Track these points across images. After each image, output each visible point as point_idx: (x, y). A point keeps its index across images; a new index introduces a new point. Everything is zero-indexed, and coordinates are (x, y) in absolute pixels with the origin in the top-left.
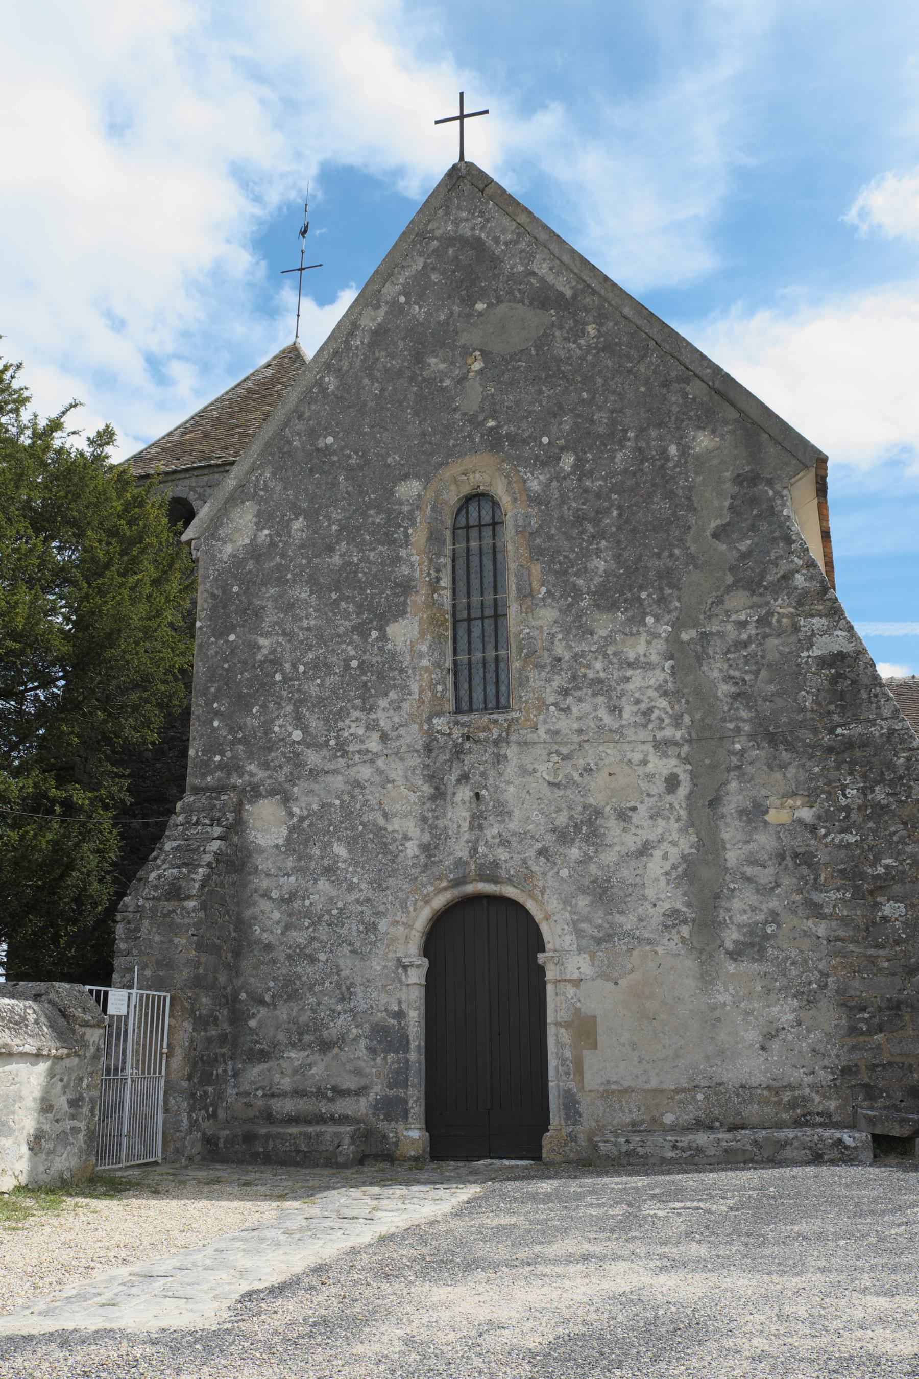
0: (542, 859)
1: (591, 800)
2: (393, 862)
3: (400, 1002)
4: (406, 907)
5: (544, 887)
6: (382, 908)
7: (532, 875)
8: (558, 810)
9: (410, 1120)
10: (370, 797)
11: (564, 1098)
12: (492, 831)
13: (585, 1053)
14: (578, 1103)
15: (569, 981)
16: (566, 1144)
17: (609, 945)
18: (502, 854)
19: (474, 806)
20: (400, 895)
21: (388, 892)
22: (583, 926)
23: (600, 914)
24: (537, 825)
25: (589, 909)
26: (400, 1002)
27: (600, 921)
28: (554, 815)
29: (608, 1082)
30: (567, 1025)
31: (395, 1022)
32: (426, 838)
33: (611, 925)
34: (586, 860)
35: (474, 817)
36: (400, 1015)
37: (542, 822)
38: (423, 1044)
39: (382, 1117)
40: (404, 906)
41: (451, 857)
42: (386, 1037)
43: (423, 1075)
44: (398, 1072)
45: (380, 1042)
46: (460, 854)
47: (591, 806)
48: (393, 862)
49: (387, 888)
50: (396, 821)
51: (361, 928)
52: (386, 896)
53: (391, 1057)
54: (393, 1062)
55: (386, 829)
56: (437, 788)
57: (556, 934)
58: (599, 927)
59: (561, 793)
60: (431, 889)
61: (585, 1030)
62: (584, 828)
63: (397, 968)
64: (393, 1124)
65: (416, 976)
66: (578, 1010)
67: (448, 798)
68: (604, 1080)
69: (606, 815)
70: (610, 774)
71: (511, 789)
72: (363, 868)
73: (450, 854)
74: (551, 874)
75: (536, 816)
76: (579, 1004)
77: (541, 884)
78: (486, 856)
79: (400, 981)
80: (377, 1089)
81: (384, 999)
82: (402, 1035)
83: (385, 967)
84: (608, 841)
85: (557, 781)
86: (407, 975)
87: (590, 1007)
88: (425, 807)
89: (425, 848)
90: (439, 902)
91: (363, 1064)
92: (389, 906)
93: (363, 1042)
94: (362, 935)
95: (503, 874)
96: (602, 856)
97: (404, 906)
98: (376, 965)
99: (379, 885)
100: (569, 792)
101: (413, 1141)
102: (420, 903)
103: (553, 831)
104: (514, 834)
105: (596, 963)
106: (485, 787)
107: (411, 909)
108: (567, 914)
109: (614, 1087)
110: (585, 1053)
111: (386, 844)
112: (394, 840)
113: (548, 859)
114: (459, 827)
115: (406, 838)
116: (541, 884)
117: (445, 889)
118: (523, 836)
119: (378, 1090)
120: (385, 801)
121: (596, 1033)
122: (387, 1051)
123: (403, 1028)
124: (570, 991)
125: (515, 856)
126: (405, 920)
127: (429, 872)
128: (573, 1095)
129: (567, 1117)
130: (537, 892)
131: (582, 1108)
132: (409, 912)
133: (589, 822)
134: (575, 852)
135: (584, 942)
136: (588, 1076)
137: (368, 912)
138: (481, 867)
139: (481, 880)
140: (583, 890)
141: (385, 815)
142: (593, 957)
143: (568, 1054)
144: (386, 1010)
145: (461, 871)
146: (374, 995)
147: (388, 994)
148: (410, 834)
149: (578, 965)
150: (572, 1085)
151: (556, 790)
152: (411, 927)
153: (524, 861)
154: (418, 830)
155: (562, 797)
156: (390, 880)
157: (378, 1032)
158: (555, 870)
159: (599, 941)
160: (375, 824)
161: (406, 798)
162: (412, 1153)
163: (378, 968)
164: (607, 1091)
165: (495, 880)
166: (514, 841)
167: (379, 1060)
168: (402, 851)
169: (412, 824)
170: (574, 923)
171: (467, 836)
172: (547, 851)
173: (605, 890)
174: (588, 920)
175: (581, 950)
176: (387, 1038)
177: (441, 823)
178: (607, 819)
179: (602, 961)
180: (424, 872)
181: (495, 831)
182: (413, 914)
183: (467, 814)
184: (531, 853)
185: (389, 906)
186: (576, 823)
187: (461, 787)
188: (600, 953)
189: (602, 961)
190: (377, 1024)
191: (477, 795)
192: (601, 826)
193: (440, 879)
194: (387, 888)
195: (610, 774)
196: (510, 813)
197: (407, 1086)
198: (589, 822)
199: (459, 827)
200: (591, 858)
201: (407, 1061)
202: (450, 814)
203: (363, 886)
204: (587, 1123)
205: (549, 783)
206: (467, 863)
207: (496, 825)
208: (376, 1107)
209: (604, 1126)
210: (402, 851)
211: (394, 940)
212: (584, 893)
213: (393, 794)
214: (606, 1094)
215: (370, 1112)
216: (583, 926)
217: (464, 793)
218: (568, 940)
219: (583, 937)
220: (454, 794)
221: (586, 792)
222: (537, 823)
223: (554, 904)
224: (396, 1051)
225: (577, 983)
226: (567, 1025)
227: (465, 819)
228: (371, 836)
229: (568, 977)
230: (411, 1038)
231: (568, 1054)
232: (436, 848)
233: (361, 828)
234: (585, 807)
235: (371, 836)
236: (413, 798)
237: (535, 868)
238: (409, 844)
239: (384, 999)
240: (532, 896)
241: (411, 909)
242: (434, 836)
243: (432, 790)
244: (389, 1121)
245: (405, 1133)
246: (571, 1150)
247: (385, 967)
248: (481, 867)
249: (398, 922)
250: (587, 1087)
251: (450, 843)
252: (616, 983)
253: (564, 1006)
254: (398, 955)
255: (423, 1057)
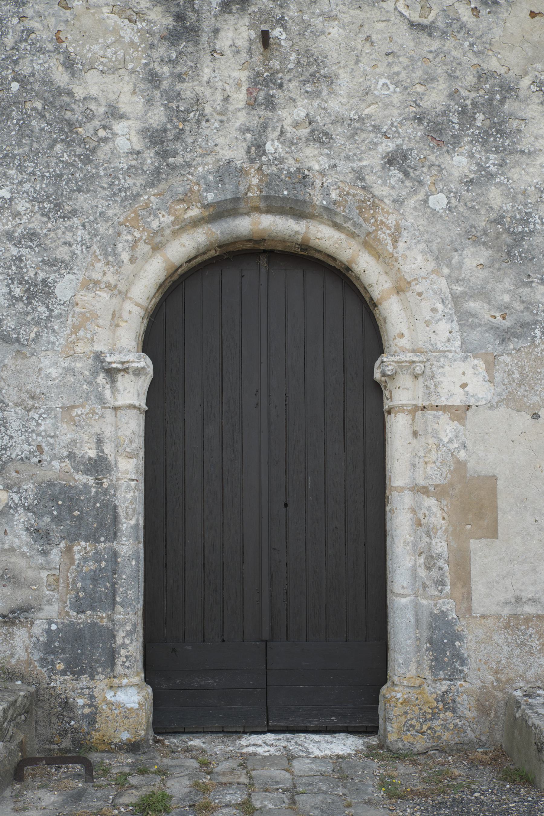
0: (395, 172)
1: (493, 64)
2: (87, 160)
3: (100, 442)
4: (115, 254)
5: (398, 228)
6: (62, 253)
7: (375, 203)
8: (429, 80)
9: (119, 669)
10: (35, 24)
11: (431, 628)
12: (294, 112)
13: (474, 544)
14: (459, 637)
15: (445, 408)
16: (435, 716)
17: (523, 344)
18: (314, 159)
19: (257, 58)
20: (102, 227)
21: (76, 221)
22: (472, 305)
23: (508, 283)
24: (386, 106)
25: (486, 273)
26: (100, 442)
27: (506, 298)
28: (420, 89)
29: (518, 600)
30: (440, 492)
31: (91, 480)
32: (157, 117)
33: (529, 305)
34: (481, 179)
35: (257, 81)
36: (99, 466)
37: (396, 99)
38: (141, 522)
39: (60, 666)
40: (109, 250)
41: (210, 159)
42: (71, 510)
43: (142, 579)
44: (95, 577)
45: (57, 520)
46: (227, 154)
47: (493, 74)
48: (87, 160)
49: (74, 212)
50: (91, 77)
51: (17, 291)
52: (70, 229)
53: (81, 548)
54: (85, 559)
55: (70, 93)
56: (180, 17)
57: (418, 321)
58: (505, 310)
59: (435, 45)
60: (168, 219)
61: (475, 503)
62: (480, 117)
63: (95, 374)
64: (85, 681)
65: (133, 392)
66: (461, 465)
67: (204, 39)
68: (510, 596)
69: (522, 94)
70: (533, 15)
71: (335, 30)
72: (21, 169)
73: (208, 153)
74: (412, 202)
75: (382, 86)
76: (462, 455)
77: (391, 220)
78: (282, 160)
79: (101, 399)
80: (51, 610)
81: (66, 434)
82: (105, 506)
83: (69, 370)
84: (525, 144)
85: (425, 22)
86: (114, 390)
87: (484, 459)
88: (155, 54)
89: (155, 138)
90: (183, 248)
91: (21, 563)
92: (77, 249)
93: (21, 518)
94: (20, 306)
95: (317, 198)
96: (514, 174)
97: (109, 250)
98: (49, 366)
99: (57, 208)
100: (450, 43)
101: (127, 713)
102: (144, 248)
103: (419, 119)
104: (338, 120)
105: (498, 376)
106: (281, 22)
107: (125, 257)
108: (443, 283)
109: (529, 609)
110: (474, 544)
111: (70, 124)
112: (89, 116)
113: (406, 174)
114: (227, 99)
115: (114, 113)
116: (391, 220)
117: (196, 223)
118: (356, 126)
119: (53, 612)
120: (68, 35)
121: (494, 508)
122: (72, 537)
123: (106, 492)
124: (447, 428)
125: (342, 165)
126: (111, 278)
127: (162, 186)
128: (450, 624)
129: (438, 664)
130: (384, 236)
131: (467, 647)
132: (120, 264)
133: (490, 107)
134: (459, 163)
135: (475, 336)
136: (479, 588)
137: (32, 259)
138: (271, 181)
139: (269, 211)
140: (473, 237)
141: (69, 64)
142: (491, 364)
143: (440, 546)
144: (71, 456)
145: (230, 187)
146: (46, 425)
147: (75, 423)
148: (124, 108)
149: (463, 379)
150: (448, 606)
151: (425, 39)
152: (124, 295)
153: (359, 175)
154: (139, 100)
155: (437, 53)
156: (81, 197)
157: (54, 499)
158: (421, 196)
159: (504, 336)
160: (47, 82)
161: (115, 31)
162: (125, 736)
163: (54, 372)
164: (515, 616)
165: (297, 210)
166: (339, 134)
167: (55, 555)
168: (105, 140)
169: (128, 88)
170: (456, 299)
171: (242, 118)
172: (405, 157)
173: (519, 239)
174: (482, 293)
175: (467, 351)
176: (70, 512)
177: (187, 89)
178: (525, 101)
179: (510, 373)
180: (152, 185)
181: (300, 113)
182: (128, 268)
183: (244, 75)
184: (373, 161)
185: (77, 249)
186: (464, 107)
187: (231, 19)
188: (506, 358)
189: (510, 373)
190: (50, 484)
191: (265, 37)
192: (512, 116)
193: (186, 199)
194: (74, 212)
195: (533, 15)
196: (330, 79)
197: (114, 603)
198: (490, 107)
199: (227, 99)
200: (492, 176)
201: (115, 555)
202: (206, 72)
203: (22, 206)
204: (477, 676)
205: (412, 25)
206: (242, 172)
207: (302, 102)
208: (49, 648)
209: (509, 681)
210: (105, 140)
211: (89, 317)
212: (476, 241)
213: (87, 21)
214: (514, 623)
215: (37, 656)
216: (472, 305)
217: (237, 33)
218: (444, 331)
219: (473, 327)
220: (216, 31)
221: (483, 47)
222: (387, 103)
223: (414, 260)
224: (93, 538)
225: (460, 413)
226: (440, 492)
227: (239, 85)
228: (39, 105)
229: (443, 401)
230: (121, 511)
231: (440, 546)
232: (177, 138)
233: (15, 86)
234: (482, 76)
235: (39, 105)
236: (129, 33)
237: (380, 190)
238: (119, 127)
239: (66, 434)
240: (370, 245)
241: (125, 257)
242: (175, 114)
243: (169, 21)
244: (77, 675)
245: (109, 696)
246: (445, 727)
247: (69, 370)
248: (271, 181)
249: (97, 283)
250: (478, 609)
251: (206, 129)
252: (536, 416)
253: (434, 456)
254: (98, 348)
255: (141, 545)
